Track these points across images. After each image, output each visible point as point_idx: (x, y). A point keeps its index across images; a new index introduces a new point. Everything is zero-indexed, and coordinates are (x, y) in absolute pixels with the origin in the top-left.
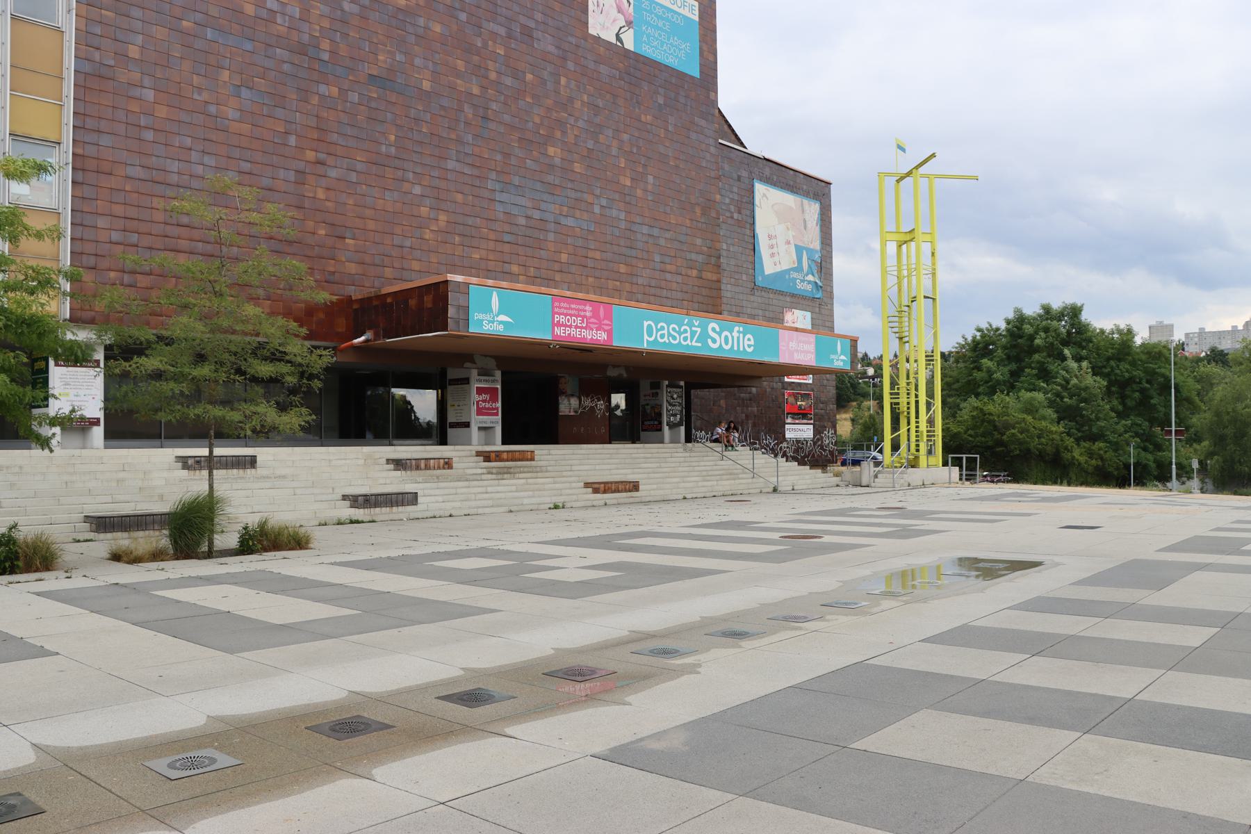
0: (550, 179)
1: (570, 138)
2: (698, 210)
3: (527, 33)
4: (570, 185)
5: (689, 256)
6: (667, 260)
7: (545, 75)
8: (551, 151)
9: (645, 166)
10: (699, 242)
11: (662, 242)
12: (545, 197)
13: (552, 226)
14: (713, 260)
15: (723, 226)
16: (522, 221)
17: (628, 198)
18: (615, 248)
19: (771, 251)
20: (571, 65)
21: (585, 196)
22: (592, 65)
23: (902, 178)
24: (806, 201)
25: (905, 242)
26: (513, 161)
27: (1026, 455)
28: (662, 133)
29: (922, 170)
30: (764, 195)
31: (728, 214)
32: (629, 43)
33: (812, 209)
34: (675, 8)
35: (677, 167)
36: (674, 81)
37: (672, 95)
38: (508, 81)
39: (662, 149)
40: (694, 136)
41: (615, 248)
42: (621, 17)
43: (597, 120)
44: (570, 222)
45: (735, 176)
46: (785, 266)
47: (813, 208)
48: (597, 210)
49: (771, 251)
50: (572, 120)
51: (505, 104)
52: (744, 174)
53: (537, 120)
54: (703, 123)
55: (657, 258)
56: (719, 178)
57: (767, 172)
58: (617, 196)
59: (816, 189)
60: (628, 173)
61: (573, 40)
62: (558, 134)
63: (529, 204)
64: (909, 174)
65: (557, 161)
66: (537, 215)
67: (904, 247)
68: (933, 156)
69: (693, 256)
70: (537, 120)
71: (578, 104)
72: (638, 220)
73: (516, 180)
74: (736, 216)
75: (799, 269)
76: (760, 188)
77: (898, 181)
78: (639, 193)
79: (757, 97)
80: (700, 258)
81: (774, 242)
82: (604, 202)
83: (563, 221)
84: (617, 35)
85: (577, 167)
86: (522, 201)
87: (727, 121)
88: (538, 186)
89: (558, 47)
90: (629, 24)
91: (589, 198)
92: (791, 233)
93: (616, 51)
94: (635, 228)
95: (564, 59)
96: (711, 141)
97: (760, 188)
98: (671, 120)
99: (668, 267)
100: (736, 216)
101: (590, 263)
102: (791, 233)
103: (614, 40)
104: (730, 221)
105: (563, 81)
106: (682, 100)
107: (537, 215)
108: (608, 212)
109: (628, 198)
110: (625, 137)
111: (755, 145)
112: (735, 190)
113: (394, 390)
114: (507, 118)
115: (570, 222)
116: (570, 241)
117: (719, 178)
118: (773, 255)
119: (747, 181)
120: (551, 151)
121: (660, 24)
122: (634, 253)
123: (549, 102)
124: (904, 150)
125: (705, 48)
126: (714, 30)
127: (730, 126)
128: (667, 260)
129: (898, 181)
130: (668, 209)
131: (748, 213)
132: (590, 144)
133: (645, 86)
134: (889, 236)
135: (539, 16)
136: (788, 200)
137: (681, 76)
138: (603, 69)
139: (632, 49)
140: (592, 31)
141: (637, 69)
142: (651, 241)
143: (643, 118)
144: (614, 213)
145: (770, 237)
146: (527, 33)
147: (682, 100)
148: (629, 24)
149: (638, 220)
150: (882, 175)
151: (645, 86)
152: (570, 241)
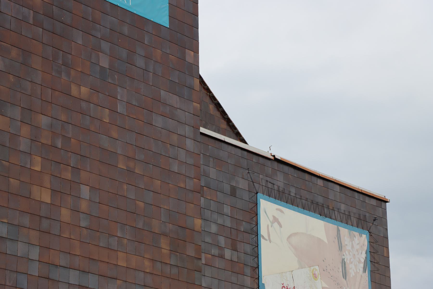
2: (164, 244)
9: (76, 170)
15: (208, 271)
17: (45, 224)
24: (344, 231)
27: (215, 104)
30: (275, 220)
31: (215, 251)
33: (357, 243)
35: (130, 171)
36: (126, 30)
37: (124, 54)
39: (105, 142)
40: (158, 121)
45: (227, 188)
47: (357, 243)
54: (174, 100)
56: (199, 191)
57: (280, 181)
58: (26, 221)
59: (361, 210)
60: (47, 180)
72: (63, 260)
74: (228, 254)
76: (268, 208)
78: (65, 214)
87: (213, 98)
94: (55, 274)
96: (188, 131)
97: (268, 208)
100: (228, 254)
104: (218, 263)
106: (140, 62)
109: (45, 224)
110: (44, 121)
111: (259, 138)
112: (227, 210)
113: (201, 128)
117: (199, 191)
119: (246, 196)
127: (218, 106)
130: (114, 242)
131: (248, 248)
133: (79, 38)
136: (316, 227)
137: (139, 22)
143: (74, 91)
144: (21, 249)
147: (140, 62)
149: (63, 260)
151: (79, 38)
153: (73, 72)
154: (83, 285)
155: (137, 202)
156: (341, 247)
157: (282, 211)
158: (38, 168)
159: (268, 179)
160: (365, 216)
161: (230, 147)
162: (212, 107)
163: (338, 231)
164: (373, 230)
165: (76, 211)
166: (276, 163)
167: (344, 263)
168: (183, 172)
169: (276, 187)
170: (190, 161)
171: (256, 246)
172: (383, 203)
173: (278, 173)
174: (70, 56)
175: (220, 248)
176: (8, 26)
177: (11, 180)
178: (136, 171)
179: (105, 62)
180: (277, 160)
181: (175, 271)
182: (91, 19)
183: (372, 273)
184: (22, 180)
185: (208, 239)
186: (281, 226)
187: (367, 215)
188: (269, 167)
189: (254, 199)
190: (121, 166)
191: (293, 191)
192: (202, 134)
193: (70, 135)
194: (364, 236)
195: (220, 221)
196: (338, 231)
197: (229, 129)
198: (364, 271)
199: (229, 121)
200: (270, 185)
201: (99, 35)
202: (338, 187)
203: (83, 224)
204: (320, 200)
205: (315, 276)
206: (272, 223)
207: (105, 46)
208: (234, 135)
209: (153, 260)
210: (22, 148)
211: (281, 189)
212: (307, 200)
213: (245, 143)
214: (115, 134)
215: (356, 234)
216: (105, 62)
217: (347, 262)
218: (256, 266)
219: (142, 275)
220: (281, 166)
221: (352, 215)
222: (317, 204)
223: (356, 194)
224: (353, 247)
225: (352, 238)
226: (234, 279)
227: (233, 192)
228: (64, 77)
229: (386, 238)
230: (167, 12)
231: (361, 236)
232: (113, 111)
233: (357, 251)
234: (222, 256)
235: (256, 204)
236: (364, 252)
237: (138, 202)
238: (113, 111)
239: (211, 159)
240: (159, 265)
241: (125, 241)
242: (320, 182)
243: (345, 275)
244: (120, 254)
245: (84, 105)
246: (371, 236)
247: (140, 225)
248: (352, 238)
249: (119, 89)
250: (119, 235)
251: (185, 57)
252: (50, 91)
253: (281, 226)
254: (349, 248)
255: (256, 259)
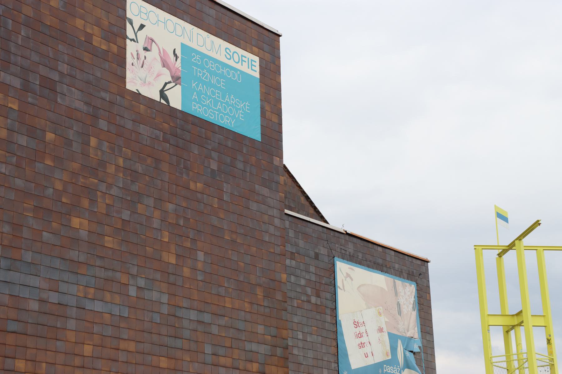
0: (73, 255)
1: (101, 208)
2: (259, 292)
3: (49, 85)
4: (98, 263)
5: (248, 346)
6: (221, 351)
7: (71, 135)
8: (76, 222)
9: (194, 240)
10: (260, 329)
11: (215, 330)
12: (65, 276)
13: (73, 312)
14: (279, 351)
16: (34, 306)
17: (172, 279)
18: (155, 338)
19: (359, 341)
20: (103, 124)
21: (118, 275)
22: (129, 125)
23: (504, 251)
25: (513, 327)
26: (26, 233)
28: (215, 203)
29: (526, 241)
30: (348, 275)
31: (304, 298)
32: (176, 99)
33: (408, 291)
34: (231, 63)
35: (234, 241)
36: (229, 144)
37: (228, 160)
38: (23, 140)
39: (215, 221)
40: (254, 206)
41: (155, 338)
42: (166, 71)
43: (135, 187)
44: (98, 306)
45: (312, 254)
46: (379, 358)
48: (133, 292)
49: (359, 341)
50: (103, 187)
51: (18, 166)
52: (323, 251)
53: (59, 186)
54: (265, 191)
55: (208, 349)
57: (350, 248)
58: (158, 276)
59: (410, 268)
60: (173, 248)
61: (107, 96)
62: (85, 203)
63: (45, 285)
64: (512, 246)
65: (83, 234)
66: (54, 298)
67: (512, 333)
68: (537, 223)
69: (254, 347)
70: (59, 186)
71: (111, 169)
73: (28, 256)
74: (313, 299)
75: (393, 362)
76: (342, 268)
77: (500, 255)
78: (186, 272)
79: (339, 162)
80: (263, 349)
81: (362, 329)
82: (141, 283)
83: (89, 305)
84: (162, 92)
85: (109, 242)
86: (35, 281)
87: (303, 193)
88: (57, 263)
89: (87, 104)
90: (176, 79)
91: (124, 279)
92: (383, 319)
93: (160, 110)
94: (180, 313)
95: (96, 117)
96: (275, 212)
97: (342, 268)
98: (226, 187)
99: (222, 360)
100: (313, 299)
101: (122, 357)
102: (383, 319)
103: (156, 97)
104: (306, 306)
105: (93, 142)
106: (240, 165)
107: (54, 298)
108: (147, 295)
109: (172, 279)
110: (170, 207)
111: (336, 221)
112: (312, 269)
114: (19, 183)
115: (98, 306)
116: (96, 329)
118: (362, 345)
119: (326, 259)
120: (76, 222)
121: (214, 81)
122: (179, 343)
123: (75, 166)
124: (505, 219)
125: (267, 108)
126: (278, 88)
127: (307, 198)
128: (221, 351)
129: (500, 255)
130: (222, 291)
131: (328, 296)
132: (126, 215)
134: (492, 321)
135: (64, 68)
136: (378, 280)
137: (239, 138)
138: (143, 129)
139: (179, 107)
140: (130, 86)
141: (183, 131)
142: (200, 328)
143: (192, 186)
144: (155, 295)
145: (356, 324)
146: (49, 85)
147: (240, 165)
148: (176, 79)
149: (185, 303)
150: (479, 248)
151: (195, 149)
152: (96, 329)
153: (191, 173)
154: (200, 320)
155: (239, 263)
156: (396, 294)
157: (353, 270)
158: (166, 240)
159: (342, 247)
160: (413, 272)
161: (314, 225)
162: (303, 199)
163: (395, 282)
164: (419, 281)
165: (194, 269)
166: (347, 236)
167: (399, 304)
168: (273, 241)
169: (348, 253)
170: (278, 234)
171: (335, 294)
172: (426, 263)
173: (349, 243)
174: (189, 162)
175: (308, 295)
176: (145, 143)
177: (147, 248)
178: (238, 241)
179: (214, 166)
180: (348, 234)
181: (267, 310)
182: (108, 100)
183: (420, 311)
184: (155, 248)
185: (299, 290)
186: (352, 280)
187: (415, 271)
188: (343, 239)
189: (332, 261)
190: (226, 237)
191: (360, 255)
192: (286, 214)
193: (189, 217)
194: (413, 286)
195: (307, 277)
196: (395, 282)
197: (315, 213)
198: (414, 309)
199: (315, 208)
200: (343, 252)
201: (210, 148)
202: (393, 252)
203: (200, 278)
204: (380, 261)
205: (380, 314)
206: (346, 278)
207: (214, 155)
208: (319, 218)
209: (251, 303)
210: (155, 226)
211: (351, 254)
212: (370, 261)
213: (328, 223)
214: (222, 216)
215: (408, 284)
216: (214, 166)
217: (401, 303)
218: (334, 308)
219: (243, 313)
220: (352, 238)
221: (404, 271)
222: (378, 264)
223: (406, 257)
224: (405, 293)
225: (404, 287)
226: (318, 317)
227: (317, 256)
228: (185, 176)
229: (428, 287)
230: (260, 131)
231: (411, 286)
232: (221, 199)
233: (408, 296)
234: (309, 301)
235: (334, 265)
236: (413, 297)
237: (239, 263)
238: (221, 199)
239: (300, 234)
240: (255, 306)
241: (231, 290)
242: (380, 249)
243: (400, 313)
244: (227, 299)
245: (199, 195)
246: (417, 286)
247: (241, 279)
248: (404, 287)
249: (225, 185)
250: (226, 285)
251: (273, 161)
252: (174, 186)
253: (352, 280)
254: (402, 294)
255: (334, 303)
